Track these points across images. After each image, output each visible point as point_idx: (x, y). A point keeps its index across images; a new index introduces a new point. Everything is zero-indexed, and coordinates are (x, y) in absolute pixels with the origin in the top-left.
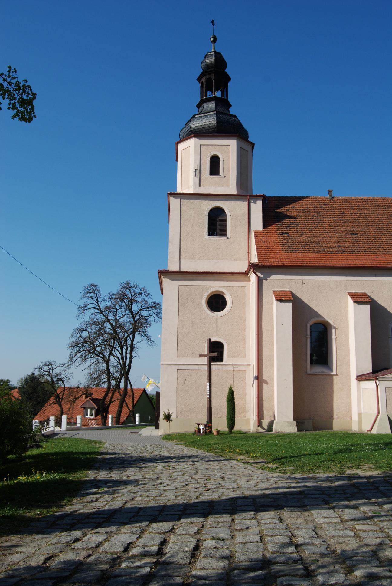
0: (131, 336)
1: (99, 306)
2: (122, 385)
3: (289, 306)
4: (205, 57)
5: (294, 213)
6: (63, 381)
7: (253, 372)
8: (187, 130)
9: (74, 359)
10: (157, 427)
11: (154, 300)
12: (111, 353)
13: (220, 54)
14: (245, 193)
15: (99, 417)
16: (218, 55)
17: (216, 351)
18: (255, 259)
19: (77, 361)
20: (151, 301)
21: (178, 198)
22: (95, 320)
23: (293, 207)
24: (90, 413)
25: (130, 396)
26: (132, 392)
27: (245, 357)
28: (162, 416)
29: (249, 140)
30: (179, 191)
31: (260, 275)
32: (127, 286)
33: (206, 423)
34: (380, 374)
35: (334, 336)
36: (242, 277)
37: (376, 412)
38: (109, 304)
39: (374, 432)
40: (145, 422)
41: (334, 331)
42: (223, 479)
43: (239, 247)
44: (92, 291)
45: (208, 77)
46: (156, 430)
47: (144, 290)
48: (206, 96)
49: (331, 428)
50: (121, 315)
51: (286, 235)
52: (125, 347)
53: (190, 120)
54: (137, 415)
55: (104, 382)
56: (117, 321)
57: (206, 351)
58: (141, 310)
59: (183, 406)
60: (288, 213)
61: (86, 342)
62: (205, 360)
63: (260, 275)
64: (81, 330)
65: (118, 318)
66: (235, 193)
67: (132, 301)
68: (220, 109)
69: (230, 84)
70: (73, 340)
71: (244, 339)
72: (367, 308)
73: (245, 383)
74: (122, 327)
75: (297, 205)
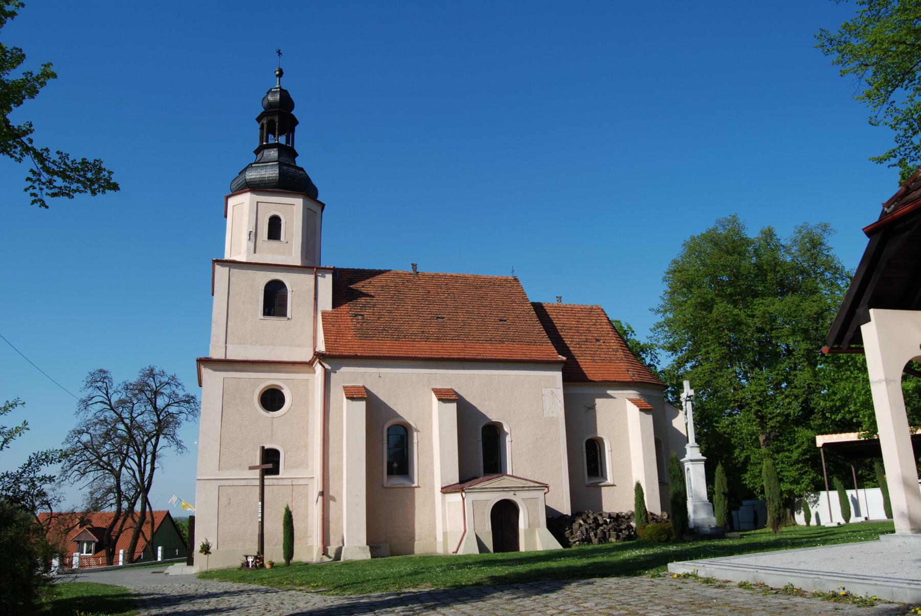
0: (153, 440)
1: (110, 400)
2: (138, 508)
3: (362, 405)
4: (268, 93)
5: (369, 290)
6: (49, 505)
7: (317, 487)
8: (240, 180)
9: (69, 473)
10: (190, 562)
11: (187, 392)
12: (123, 465)
13: (286, 91)
14: (311, 264)
15: (103, 552)
16: (284, 94)
17: (270, 461)
18: (321, 348)
19: (73, 476)
20: (184, 393)
21: (226, 266)
22: (102, 418)
23: (370, 282)
24: (87, 549)
25: (148, 522)
26: (152, 516)
27: (307, 468)
28: (197, 547)
29: (319, 199)
30: (227, 257)
31: (327, 366)
32: (151, 374)
33: (256, 554)
34: (466, 485)
35: (415, 441)
36: (306, 368)
37: (463, 530)
38: (123, 397)
39: (460, 552)
40: (170, 557)
41: (415, 434)
42: (282, 603)
44: (100, 378)
45: (270, 118)
46: (190, 567)
47: (173, 378)
48: (267, 141)
49: (413, 553)
50: (139, 411)
51: (360, 317)
52: (144, 456)
53: (245, 170)
54: (160, 548)
55: (111, 505)
56: (132, 419)
57: (257, 461)
58: (168, 405)
59: (224, 532)
60: (364, 290)
61: (86, 448)
62: (257, 474)
63: (327, 366)
64: (81, 432)
65: (134, 415)
66: (299, 264)
67: (156, 393)
68: (283, 159)
69: (297, 128)
70: (69, 446)
71: (306, 446)
72: (453, 406)
73: (307, 501)
74: (140, 428)
75: (375, 280)
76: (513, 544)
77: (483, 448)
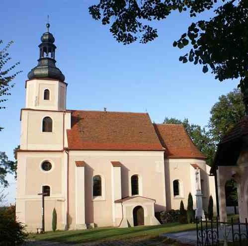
14: (62, 109)
16: (50, 35)
17: (46, 191)
18: (66, 146)
37: (122, 217)
39: (120, 227)
43: (58, 138)
49: (144, 224)
62: (41, 196)
69: (56, 50)
76: (142, 223)
77: (131, 185)
